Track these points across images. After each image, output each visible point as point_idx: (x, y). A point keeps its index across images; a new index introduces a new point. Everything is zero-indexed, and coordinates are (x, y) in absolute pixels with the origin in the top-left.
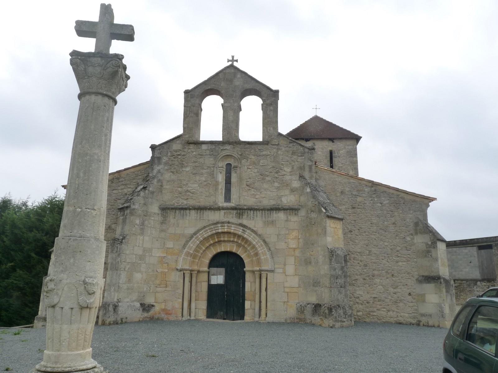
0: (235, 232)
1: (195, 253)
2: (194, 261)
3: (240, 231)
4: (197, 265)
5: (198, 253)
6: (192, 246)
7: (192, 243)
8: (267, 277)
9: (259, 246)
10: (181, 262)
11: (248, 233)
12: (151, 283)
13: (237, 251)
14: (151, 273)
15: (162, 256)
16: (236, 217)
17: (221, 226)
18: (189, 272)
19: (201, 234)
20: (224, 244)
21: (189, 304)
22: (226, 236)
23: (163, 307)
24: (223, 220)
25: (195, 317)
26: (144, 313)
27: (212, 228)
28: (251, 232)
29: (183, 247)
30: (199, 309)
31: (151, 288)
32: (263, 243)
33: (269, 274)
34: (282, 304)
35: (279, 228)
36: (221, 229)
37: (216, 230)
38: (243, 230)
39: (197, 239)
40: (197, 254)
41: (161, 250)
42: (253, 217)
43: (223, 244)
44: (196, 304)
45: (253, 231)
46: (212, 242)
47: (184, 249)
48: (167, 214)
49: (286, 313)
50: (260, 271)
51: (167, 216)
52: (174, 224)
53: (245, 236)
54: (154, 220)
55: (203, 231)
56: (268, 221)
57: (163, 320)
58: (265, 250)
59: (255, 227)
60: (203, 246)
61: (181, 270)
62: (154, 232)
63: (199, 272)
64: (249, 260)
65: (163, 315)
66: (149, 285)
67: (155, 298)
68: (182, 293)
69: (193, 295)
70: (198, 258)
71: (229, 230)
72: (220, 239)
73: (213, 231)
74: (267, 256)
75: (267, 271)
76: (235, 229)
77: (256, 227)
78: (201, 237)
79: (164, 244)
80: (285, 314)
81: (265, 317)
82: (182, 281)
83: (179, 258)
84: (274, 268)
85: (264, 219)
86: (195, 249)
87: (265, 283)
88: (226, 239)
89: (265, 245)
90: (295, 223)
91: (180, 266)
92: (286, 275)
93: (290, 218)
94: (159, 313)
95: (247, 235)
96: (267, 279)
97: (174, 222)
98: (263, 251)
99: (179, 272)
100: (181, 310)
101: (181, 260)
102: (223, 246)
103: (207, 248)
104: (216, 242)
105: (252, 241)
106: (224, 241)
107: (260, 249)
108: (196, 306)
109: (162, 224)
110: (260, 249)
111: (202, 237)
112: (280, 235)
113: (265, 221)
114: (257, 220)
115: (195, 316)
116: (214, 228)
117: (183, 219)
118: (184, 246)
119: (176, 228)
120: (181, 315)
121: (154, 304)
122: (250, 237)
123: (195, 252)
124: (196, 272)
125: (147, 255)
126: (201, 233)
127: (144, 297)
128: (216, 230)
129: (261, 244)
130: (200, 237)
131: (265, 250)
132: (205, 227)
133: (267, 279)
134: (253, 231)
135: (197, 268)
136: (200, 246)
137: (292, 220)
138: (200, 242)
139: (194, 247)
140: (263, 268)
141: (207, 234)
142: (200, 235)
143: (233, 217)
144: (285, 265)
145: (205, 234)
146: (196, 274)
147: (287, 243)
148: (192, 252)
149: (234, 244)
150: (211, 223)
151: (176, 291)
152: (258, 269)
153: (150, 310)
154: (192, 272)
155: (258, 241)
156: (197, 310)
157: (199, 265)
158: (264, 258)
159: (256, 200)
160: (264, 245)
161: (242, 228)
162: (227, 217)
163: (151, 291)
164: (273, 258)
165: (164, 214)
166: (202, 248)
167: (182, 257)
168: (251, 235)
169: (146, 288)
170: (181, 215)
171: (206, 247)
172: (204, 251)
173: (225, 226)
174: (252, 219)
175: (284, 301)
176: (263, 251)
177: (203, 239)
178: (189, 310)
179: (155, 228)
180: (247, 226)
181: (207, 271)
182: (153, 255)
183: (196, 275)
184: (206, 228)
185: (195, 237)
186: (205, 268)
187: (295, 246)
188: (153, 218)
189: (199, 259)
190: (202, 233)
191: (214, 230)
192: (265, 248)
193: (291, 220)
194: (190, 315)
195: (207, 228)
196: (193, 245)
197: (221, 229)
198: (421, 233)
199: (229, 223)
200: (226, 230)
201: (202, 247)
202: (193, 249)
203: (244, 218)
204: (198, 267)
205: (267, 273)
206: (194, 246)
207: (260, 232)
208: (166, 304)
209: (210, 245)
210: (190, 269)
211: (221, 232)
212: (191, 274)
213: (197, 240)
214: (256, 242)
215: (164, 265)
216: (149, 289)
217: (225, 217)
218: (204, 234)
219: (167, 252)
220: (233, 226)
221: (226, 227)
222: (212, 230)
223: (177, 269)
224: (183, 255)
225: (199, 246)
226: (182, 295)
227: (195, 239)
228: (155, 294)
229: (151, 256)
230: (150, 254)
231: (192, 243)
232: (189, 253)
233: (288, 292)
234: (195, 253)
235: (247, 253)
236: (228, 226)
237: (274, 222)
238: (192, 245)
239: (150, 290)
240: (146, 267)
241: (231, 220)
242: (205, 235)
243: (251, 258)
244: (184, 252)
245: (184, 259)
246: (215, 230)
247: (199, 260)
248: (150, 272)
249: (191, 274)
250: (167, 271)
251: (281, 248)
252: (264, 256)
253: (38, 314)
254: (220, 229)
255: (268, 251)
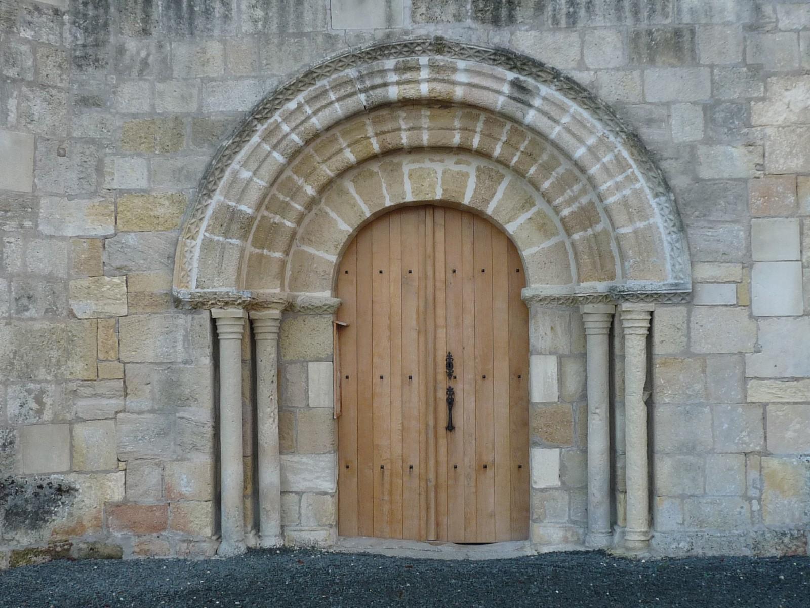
0: (477, 97)
1: (263, 217)
2: (262, 256)
3: (498, 92)
4: (281, 274)
5: (283, 217)
6: (251, 180)
7: (245, 164)
8: (650, 329)
9: (605, 168)
10: (195, 264)
11: (545, 99)
12: (42, 373)
13: (487, 201)
14: (37, 326)
15: (93, 233)
16: (476, 18)
17: (396, 70)
18: (240, 312)
19: (293, 112)
20: (416, 166)
21: (249, 474)
22: (425, 122)
23: (117, 495)
24: (406, 33)
25: (282, 534)
26: (15, 528)
27: (351, 81)
28: (559, 96)
29: (201, 185)
30: (300, 494)
31: (48, 401)
32: (625, 154)
33: (667, 317)
34: (736, 462)
35: (712, 67)
36: (398, 83)
37: (373, 87)
38: (516, 84)
39: (275, 141)
40: (277, 219)
41: (85, 202)
42: (568, 15)
43: (408, 165)
44: (282, 469)
45: (572, 87)
46: (350, 156)
47: (210, 197)
48: (107, 12)
49: (756, 507)
50: (615, 297)
51: (106, 25)
52: (145, 63)
53: (531, 117)
54: (35, 45)
55: (301, 98)
56: (650, 33)
57: (121, 558)
58: (638, 186)
59: (582, 65)
60: (307, 178)
61: (196, 306)
62: (38, 107)
63: (289, 309)
64: (547, 244)
65: (118, 534)
66: (31, 386)
67: (72, 447)
68: (210, 424)
69: (269, 429)
70: (282, 241)
71: (441, 89)
72: (391, 140)
73: (355, 98)
74: (651, 221)
75: (655, 297)
76: (476, 80)
77: (588, 69)
78: (293, 130)
79: (99, 170)
80: (752, 512)
81: (645, 533)
82: (207, 361)
83: (185, 245)
84: (694, 283)
85: (629, 22)
86: (264, 198)
87: (643, 357)
88: (425, 138)
89: (640, 163)
90: (799, 39)
91: (193, 284)
92: (751, 316)
93: (774, 11)
94: (99, 525)
95: (539, 110)
96: (650, 338)
97: (143, 54)
98: (627, 192)
99: (190, 317)
100: (209, 506)
101: (197, 253)
102: (410, 176)
103: (326, 187)
104: (374, 157)
105: (567, 141)
106: (416, 150)
107: (610, 183)
108: (283, 481)
109: (80, 66)
110: (610, 183)
111: (302, 128)
112: (718, 103)
113: (638, 35)
114: (595, 28)
115: (282, 527)
116: (361, 78)
117: (192, 34)
118: (204, 178)
119: (160, 86)
120: (208, 531)
121: (71, 479)
122: (556, 121)
123: (267, 208)
124: (276, 313)
125: (6, 228)
126: (292, 105)
127: (8, 450)
128: (373, 87)
129: (618, 158)
130: (286, 128)
131: (638, 186)
132: (310, 76)
133: (650, 338)
134: (572, 87)
135: (278, 291)
136: (289, 179)
137: (784, 23)
138: (292, 157)
139: (261, 183)
140: (634, 284)
141: (327, 112)
142: (286, 119)
143: (458, 18)
144: (751, 266)
145: (315, 113)
146: (277, 323)
147: (760, 149)
148: (247, 209)
149: (469, 164)
150: (342, 49)
151: (181, 414)
152: (601, 287)
153: (49, 512)
154: (254, 314)
155: (601, 141)
156: (292, 498)
157: (288, 273)
158: (636, 232)
159: (168, 329)
160: (631, 162)
161: (511, 76)
162: (431, 19)
163: (47, 415)
164: (682, 228)
165: (91, 12)
166: (300, 188)
167: (201, 237)
168: (563, 109)
169: (18, 403)
170: (180, 17)
171: (323, 180)
172: (312, 203)
173: (417, 68)
174: (563, 22)
175: (742, 448)
176: (627, 192)
177: (307, 143)
178: (249, 502)
179: (43, 86)
180: (540, 66)
181: (330, 306)
182: (44, 229)
183: (275, 330)
184: (319, 84)
185: (261, 128)
186: (323, 290)
187: (801, 161)
188: (27, 34)
189: (290, 245)
190: (300, 106)
191: (361, 91)
192: (640, 176)
193: (781, 26)
194: (257, 526)
195: (324, 83)
196: (254, 174)
197: (398, 83)
198: (434, 189)
199: (439, 46)
200: (424, 89)
201: (300, 181)
202: (254, 195)
203: (520, 20)
204: (283, 289)
205: (650, 307)
206: (255, 179)
207: (609, 92)
208: (130, 481)
209: (343, 173)
210: (246, 296)
211: (399, 101)
212: (251, 322)
213: (275, 147)
214: (590, 149)
215: (107, 279)
216: (35, 406)
217: (418, 18)
218: (309, 110)
219: (116, 212)
220: (461, 64)
221: (424, 74)
222: (350, 89)
223: (178, 302)
224: (204, 225)
225: (284, 176)
226: (208, 431)
227: (265, 139)
228: (71, 431)
229: (35, 233)
230: (28, 224)
231: (245, 164)
232: (234, 214)
233: (764, 406)
234: (263, 217)
235: (534, 210)
236: (433, 66)
237: (687, 36)
238: (246, 174)
239: (39, 412)
240: (10, 291)
241: (450, 32)
242: (314, 120)
243: (553, 234)
244: (209, 212)
245: (207, 245)
246: (365, 90)
247: (287, 253)
248: (32, 319)
249: (251, 322)
250: (124, 310)
251: (726, 175)
252: (631, 220)
253: (483, 123)
254: (393, 83)
255: (656, 195)
